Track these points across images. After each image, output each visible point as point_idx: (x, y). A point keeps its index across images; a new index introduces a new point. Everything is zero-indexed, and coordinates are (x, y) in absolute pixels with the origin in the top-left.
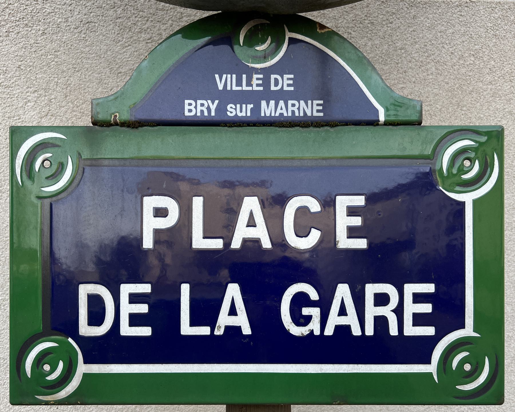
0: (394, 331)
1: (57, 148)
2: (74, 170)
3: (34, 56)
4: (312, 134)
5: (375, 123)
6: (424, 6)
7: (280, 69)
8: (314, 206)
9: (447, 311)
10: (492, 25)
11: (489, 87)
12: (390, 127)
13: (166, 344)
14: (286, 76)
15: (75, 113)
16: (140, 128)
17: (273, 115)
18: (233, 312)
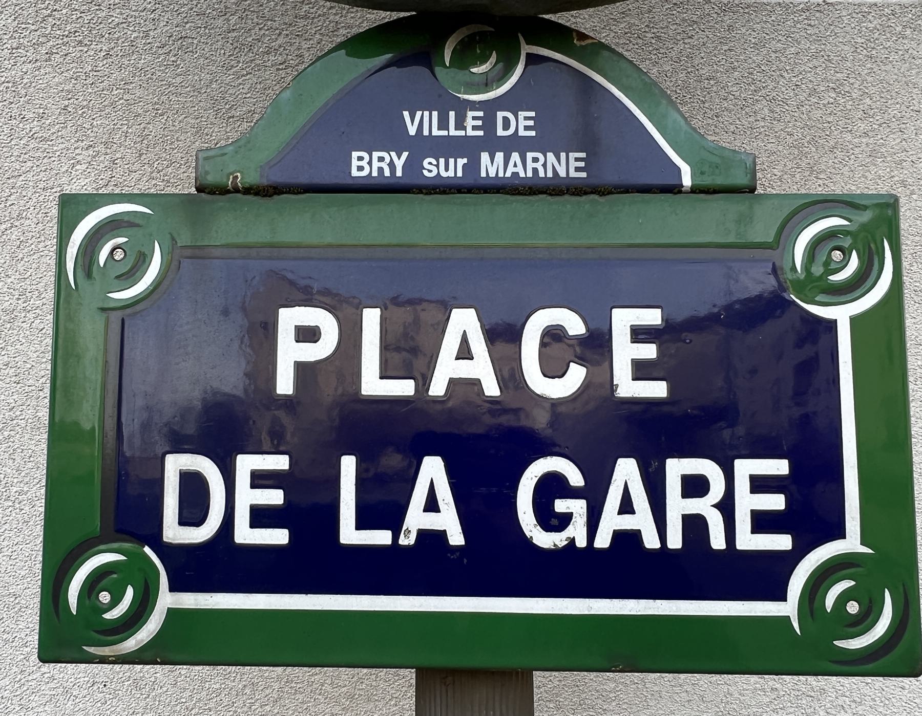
0: (718, 541)
1: (136, 229)
2: (165, 261)
3: (90, 90)
4: (568, 206)
5: (675, 189)
6: (747, 11)
7: (511, 102)
8: (575, 325)
9: (810, 513)
10: (863, 41)
11: (864, 140)
12: (702, 195)
13: (313, 558)
14: (522, 114)
15: (154, 182)
16: (275, 197)
17: (501, 175)
18: (432, 505)
